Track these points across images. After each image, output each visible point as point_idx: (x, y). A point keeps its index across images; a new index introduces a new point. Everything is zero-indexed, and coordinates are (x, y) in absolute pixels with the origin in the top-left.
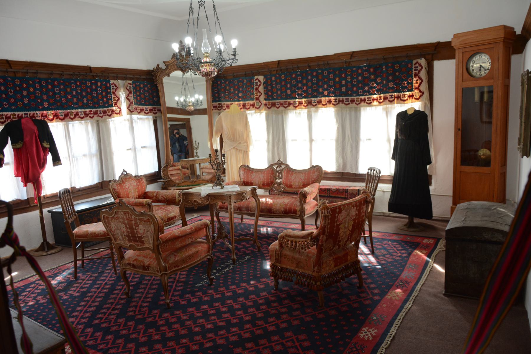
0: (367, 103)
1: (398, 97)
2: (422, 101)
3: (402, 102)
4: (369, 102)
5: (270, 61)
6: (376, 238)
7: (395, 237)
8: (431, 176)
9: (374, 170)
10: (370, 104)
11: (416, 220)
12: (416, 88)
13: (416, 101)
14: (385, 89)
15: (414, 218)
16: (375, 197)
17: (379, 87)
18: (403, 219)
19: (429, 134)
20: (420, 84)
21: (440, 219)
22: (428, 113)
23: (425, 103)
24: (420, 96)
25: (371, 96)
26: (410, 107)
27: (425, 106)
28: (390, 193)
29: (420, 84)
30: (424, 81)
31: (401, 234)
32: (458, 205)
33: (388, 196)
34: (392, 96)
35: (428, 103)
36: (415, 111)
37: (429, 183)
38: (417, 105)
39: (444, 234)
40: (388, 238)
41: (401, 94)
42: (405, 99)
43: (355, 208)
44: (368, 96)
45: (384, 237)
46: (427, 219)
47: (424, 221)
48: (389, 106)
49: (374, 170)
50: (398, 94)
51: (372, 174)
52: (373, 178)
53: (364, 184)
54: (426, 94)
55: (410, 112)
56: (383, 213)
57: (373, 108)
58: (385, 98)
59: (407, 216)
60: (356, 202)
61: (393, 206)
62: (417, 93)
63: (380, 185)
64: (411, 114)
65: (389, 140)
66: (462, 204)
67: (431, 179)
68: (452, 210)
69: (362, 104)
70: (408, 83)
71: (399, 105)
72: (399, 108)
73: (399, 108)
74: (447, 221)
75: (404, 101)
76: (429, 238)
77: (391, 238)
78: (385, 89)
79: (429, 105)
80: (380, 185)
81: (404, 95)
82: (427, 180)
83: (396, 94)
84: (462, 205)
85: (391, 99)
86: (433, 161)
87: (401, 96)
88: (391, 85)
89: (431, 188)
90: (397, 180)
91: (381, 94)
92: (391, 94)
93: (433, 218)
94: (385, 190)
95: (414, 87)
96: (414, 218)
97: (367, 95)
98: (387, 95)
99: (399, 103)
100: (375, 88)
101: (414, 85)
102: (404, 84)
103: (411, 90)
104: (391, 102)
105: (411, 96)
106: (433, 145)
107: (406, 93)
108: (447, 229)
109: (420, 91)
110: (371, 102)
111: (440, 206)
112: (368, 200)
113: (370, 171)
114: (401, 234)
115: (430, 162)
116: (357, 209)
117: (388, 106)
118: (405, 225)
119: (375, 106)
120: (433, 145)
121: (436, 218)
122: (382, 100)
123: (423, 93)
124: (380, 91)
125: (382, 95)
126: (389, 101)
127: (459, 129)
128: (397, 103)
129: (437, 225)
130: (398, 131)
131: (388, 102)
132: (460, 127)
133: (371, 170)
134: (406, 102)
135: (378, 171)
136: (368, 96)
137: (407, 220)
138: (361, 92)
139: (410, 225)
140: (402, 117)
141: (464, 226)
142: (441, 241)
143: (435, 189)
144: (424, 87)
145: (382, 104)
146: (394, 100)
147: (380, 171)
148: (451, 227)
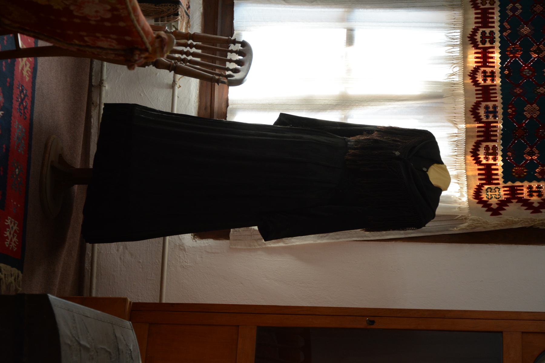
0: (475, 31)
1: (487, 134)
2: (470, 208)
3: (471, 147)
4: (478, 37)
5: (217, 303)
6: (12, 68)
7: (18, 128)
8: (226, 237)
9: (239, 63)
10: (470, 39)
11: (79, 192)
12: (513, 192)
13: (472, 192)
14: (518, 91)
15: (85, 187)
16: (152, 68)
17: (527, 72)
18: (82, 149)
19: (359, 233)
20: (527, 204)
21: (87, 265)
22: (431, 227)
23: (463, 219)
24: (486, 204)
25: (497, 44)
26: (452, 172)
27: (452, 218)
28: (169, 110)
29: (527, 204)
30: (535, 216)
31: (29, 146)
32: (128, 324)
33: (158, 101)
34: (495, 113)
35: (463, 227)
36: (438, 191)
37: (201, 232)
38: (457, 194)
39: (36, 289)
40: (16, 104)
41: (499, 144)
42: (482, 157)
43: (108, 16)
44: (497, 35)
45: (16, 92)
46: (83, 226)
47: (77, 218)
48: (461, 106)
49: (239, 63)
50: (499, 133)
51: (230, 56)
52: (219, 55)
53: (196, 28)
54: (492, 222)
55: (433, 174)
56: (100, 84)
57: (457, 51)
58: (486, 93)
59: (91, 166)
60: (128, 18)
61: (125, 117)
62: (498, 193)
63: (194, 84)
64: (427, 177)
65: (345, 102)
66: (132, 336)
67: (216, 237)
68: (112, 305)
69: (472, 15)
70: (532, 165)
71: (463, 136)
72: (449, 137)
73: (449, 137)
74: (80, 292)
75: (475, 154)
76: (22, 234)
77: (16, 114)
78: (518, 91)
79: (456, 230)
80: (194, 84)
81: (495, 154)
82: (212, 226)
83: (500, 125)
84: (128, 335)
85: (482, 112)
86: (273, 244)
87: (491, 144)
88: (531, 111)
89: (187, 239)
90: (212, 128)
91: (503, 76)
92: (500, 110)
93: (89, 245)
94: (177, 90)
95: (518, 183)
96: (85, 187)
97: (502, 29)
98: (499, 98)
99: (468, 137)
100: (526, 57)
101: (526, 184)
102: (531, 154)
103: (507, 177)
104: (473, 112)
105: (488, 174)
106: (324, 241)
107: (500, 158)
108: (51, 297)
109: (503, 204)
110: (476, 46)
111: (128, 266)
112: (133, 52)
113: (238, 47)
114: (29, 146)
115: (268, 234)
116: (103, 20)
117: (462, 100)
118: (61, 158)
119: (465, 57)
120: (324, 241)
121: (88, 252)
122: (480, 80)
123: (496, 212)
124: (510, 72)
125: (498, 81)
126: (477, 106)
127: (372, 322)
128: (467, 130)
129: (67, 258)
130: (375, 136)
131: (474, 100)
132: (380, 325)
133: (239, 53)
134: (470, 158)
135: (237, 76)
136: (497, 35)
137: (78, 164)
138: (514, 9)
139: (63, 175)
140: (422, 146)
141: (63, 348)
142: (15, 271)
143: (182, 248)
144: (515, 215)
145: (469, 81)
146: (478, 119)
147: (239, 82)
148: (57, 311)
